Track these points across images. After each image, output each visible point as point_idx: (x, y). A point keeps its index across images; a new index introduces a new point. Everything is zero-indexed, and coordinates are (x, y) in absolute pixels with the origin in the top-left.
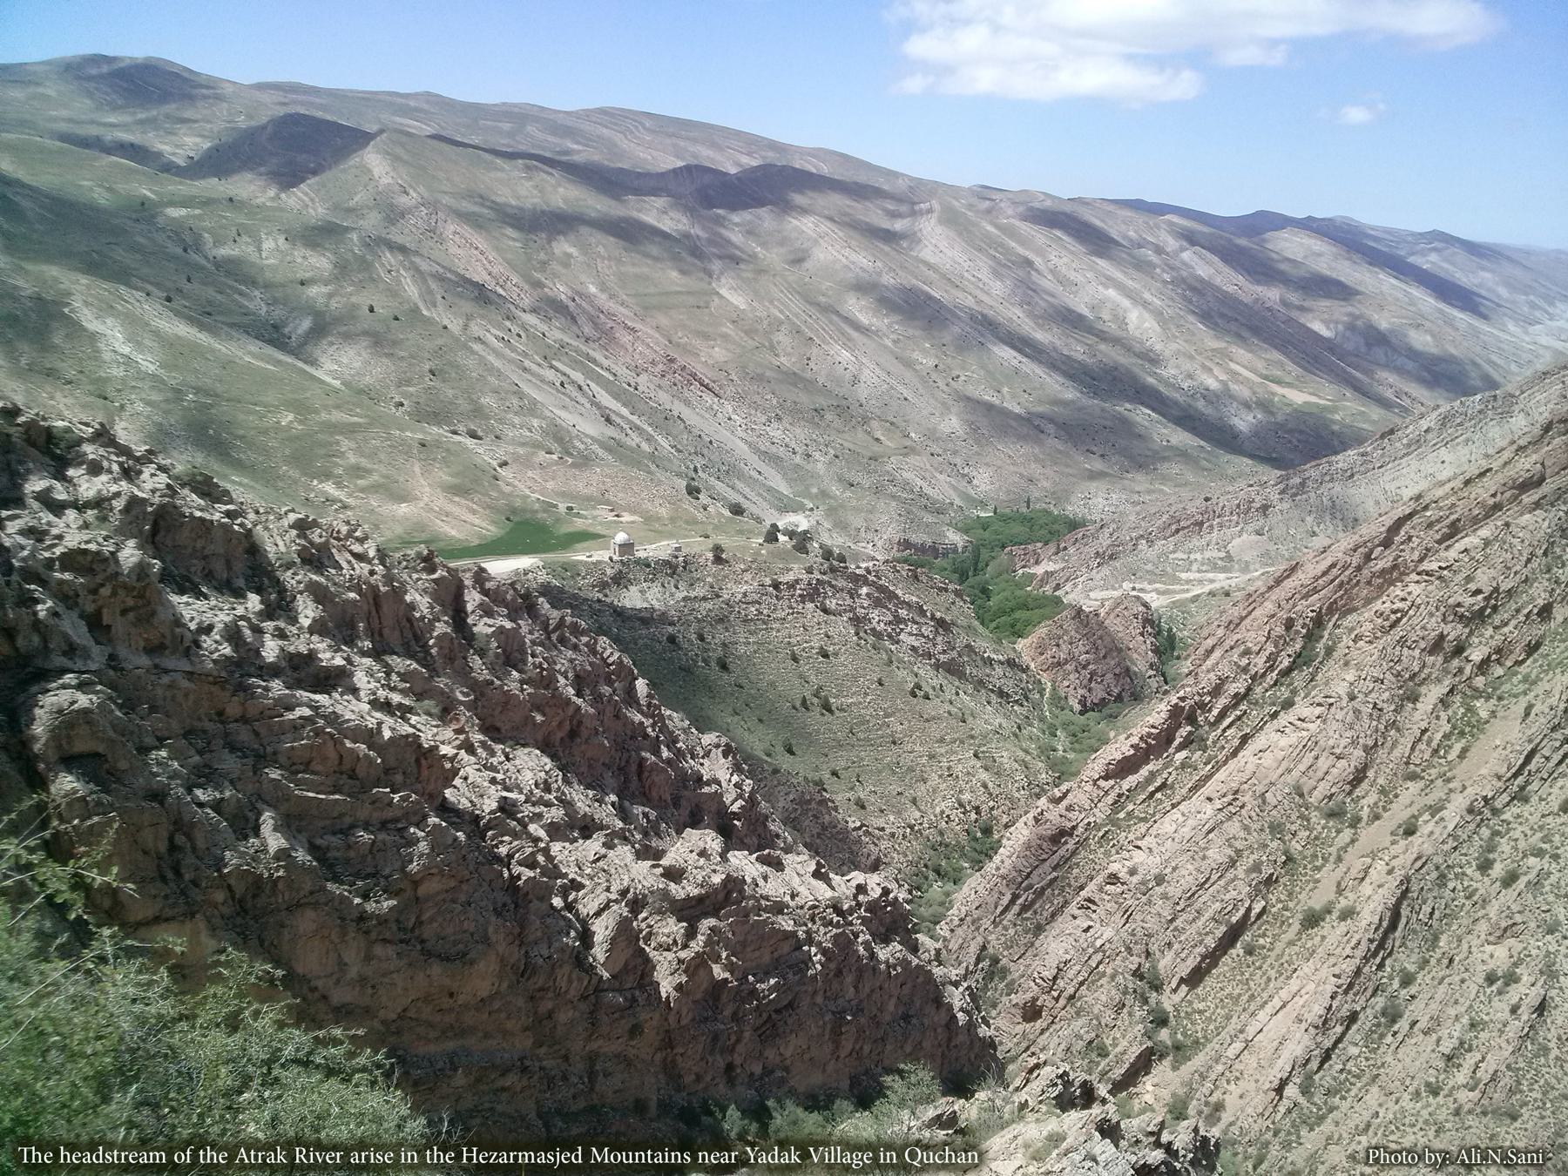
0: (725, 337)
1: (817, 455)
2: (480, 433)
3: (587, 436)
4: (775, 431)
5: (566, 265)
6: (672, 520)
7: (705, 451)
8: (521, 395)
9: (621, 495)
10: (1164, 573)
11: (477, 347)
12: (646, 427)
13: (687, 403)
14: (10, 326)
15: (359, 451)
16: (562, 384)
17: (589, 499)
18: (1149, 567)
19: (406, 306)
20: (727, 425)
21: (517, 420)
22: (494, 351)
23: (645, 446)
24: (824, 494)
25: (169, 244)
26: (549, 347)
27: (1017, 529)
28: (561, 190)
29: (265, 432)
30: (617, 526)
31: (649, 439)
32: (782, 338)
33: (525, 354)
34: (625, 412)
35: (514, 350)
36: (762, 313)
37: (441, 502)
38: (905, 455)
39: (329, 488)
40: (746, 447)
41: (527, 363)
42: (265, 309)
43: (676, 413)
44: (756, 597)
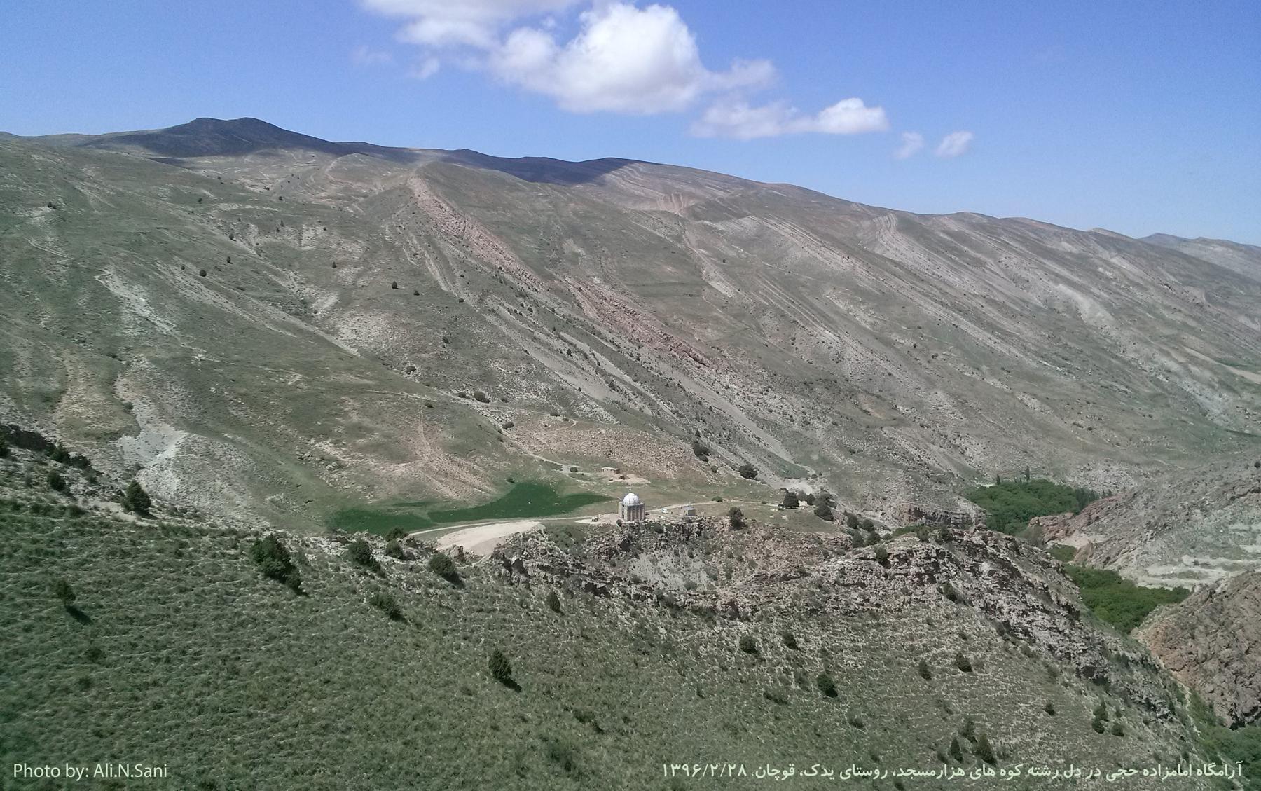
0: (716, 320)
1: (815, 422)
2: (487, 396)
3: (592, 399)
4: (773, 400)
5: (575, 263)
6: (681, 482)
7: (706, 417)
8: (529, 360)
9: (626, 457)
10: (1226, 547)
11: (490, 318)
12: (648, 393)
13: (686, 373)
14: (41, 290)
15: (363, 411)
16: (569, 352)
17: (593, 460)
18: (1208, 539)
19: (427, 284)
20: (727, 393)
21: (524, 384)
22: (507, 322)
23: (648, 411)
24: (825, 461)
25: (217, 232)
26: (558, 320)
27: (1028, 499)
28: (572, 205)
29: (269, 391)
30: (625, 489)
31: (652, 404)
32: (768, 321)
33: (534, 325)
34: (628, 379)
35: (525, 321)
36: (747, 300)
37: (441, 461)
38: (896, 426)
39: (327, 447)
40: (744, 415)
41: (536, 333)
42: (297, 288)
43: (676, 382)
44: (858, 576)
